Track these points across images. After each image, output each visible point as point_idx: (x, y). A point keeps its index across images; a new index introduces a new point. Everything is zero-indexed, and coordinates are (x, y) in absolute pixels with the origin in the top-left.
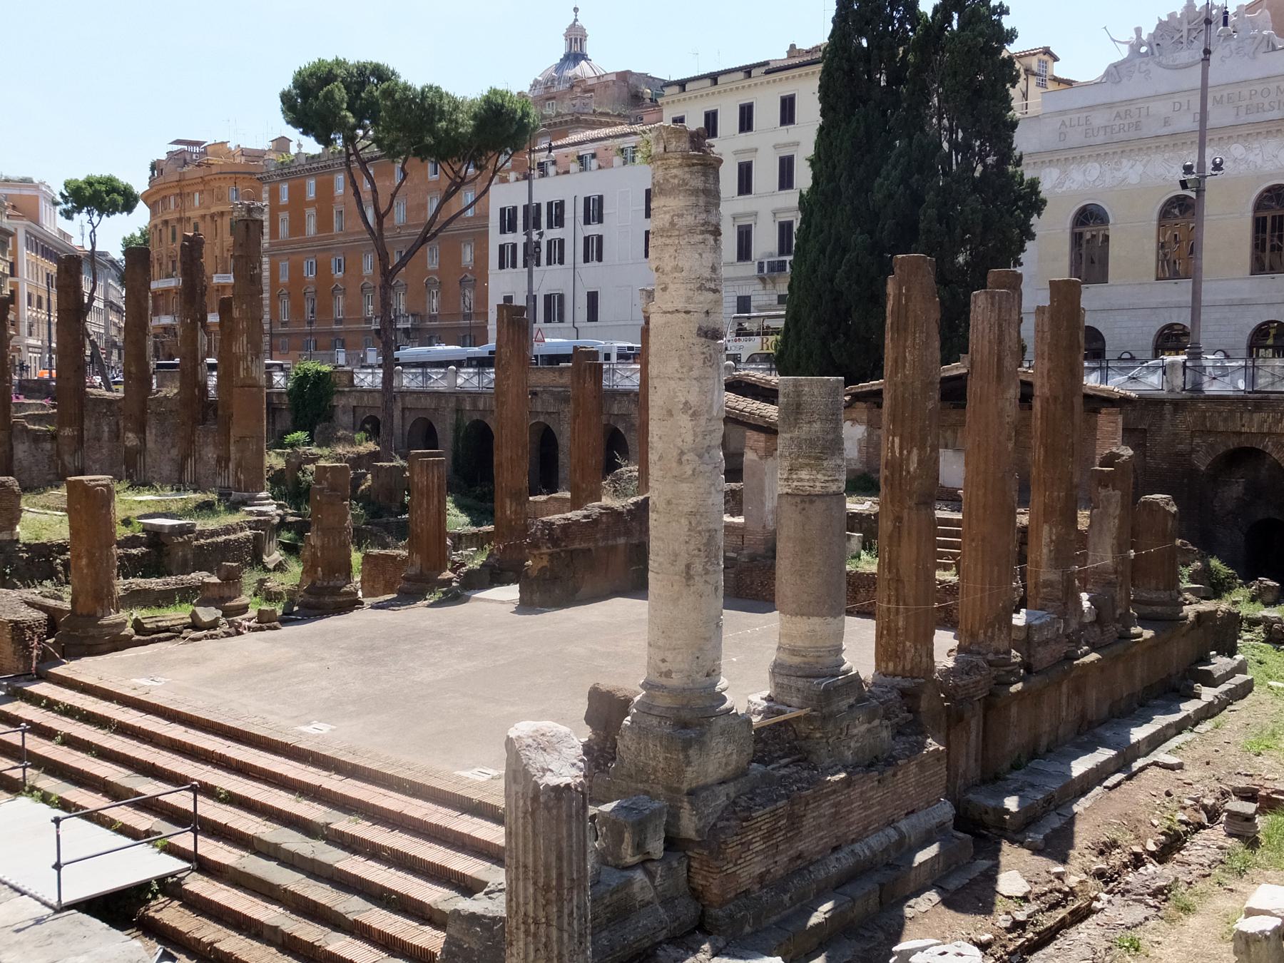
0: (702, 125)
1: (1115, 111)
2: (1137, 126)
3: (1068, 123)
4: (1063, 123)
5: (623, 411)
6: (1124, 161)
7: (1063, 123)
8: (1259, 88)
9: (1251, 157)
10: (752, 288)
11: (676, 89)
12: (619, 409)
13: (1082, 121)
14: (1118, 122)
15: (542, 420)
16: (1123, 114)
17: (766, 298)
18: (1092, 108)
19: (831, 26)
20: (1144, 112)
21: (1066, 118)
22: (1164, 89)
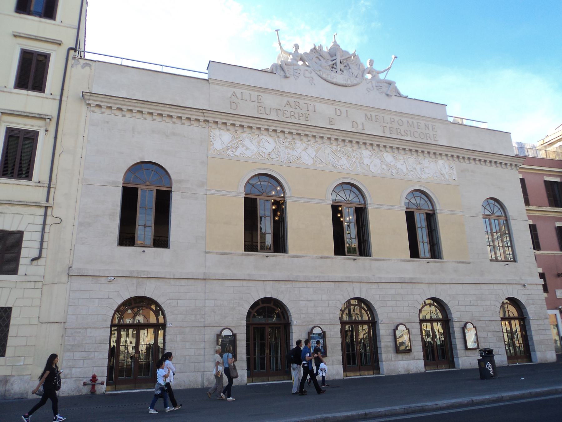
9: (399, 165)
21: (238, 91)
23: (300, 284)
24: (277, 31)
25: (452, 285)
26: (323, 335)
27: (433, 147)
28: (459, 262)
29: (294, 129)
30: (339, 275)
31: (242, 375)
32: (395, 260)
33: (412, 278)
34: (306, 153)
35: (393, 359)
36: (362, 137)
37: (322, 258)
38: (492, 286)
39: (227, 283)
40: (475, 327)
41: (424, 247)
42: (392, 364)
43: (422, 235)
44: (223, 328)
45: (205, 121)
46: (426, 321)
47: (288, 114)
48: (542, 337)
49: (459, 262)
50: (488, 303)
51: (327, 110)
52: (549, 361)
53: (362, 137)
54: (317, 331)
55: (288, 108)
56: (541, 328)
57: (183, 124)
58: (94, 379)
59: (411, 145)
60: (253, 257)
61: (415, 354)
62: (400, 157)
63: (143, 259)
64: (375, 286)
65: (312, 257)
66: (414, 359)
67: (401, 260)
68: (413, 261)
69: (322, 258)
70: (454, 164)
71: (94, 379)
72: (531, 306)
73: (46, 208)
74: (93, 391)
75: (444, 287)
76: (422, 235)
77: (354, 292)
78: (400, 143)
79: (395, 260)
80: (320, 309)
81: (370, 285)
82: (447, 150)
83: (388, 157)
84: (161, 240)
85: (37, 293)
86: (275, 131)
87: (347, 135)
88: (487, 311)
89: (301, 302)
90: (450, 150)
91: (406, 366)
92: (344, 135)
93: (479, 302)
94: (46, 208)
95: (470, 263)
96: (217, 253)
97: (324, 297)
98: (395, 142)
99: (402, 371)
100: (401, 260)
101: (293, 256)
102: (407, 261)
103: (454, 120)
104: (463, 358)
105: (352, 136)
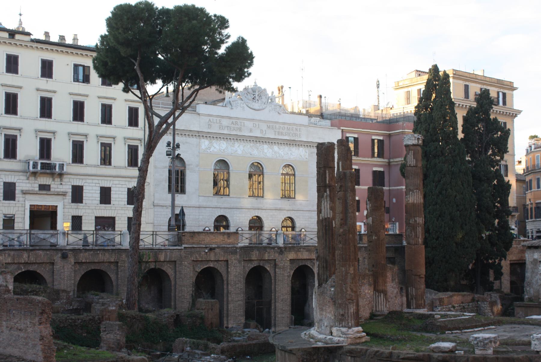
0: (515, 108)
1: (231, 120)
2: (240, 130)
3: (212, 120)
4: (210, 120)
5: (272, 257)
6: (236, 143)
7: (210, 120)
8: (282, 126)
9: (280, 152)
10: (17, 178)
11: (6, 35)
12: (269, 256)
13: (218, 121)
14: (233, 126)
15: (212, 266)
16: (234, 123)
17: (28, 185)
18: (223, 117)
19: (248, 45)
20: (242, 124)
21: (211, 118)
22: (250, 117)
39: (207, 209)
51: (249, 124)
64: (264, 211)
83: (276, 148)
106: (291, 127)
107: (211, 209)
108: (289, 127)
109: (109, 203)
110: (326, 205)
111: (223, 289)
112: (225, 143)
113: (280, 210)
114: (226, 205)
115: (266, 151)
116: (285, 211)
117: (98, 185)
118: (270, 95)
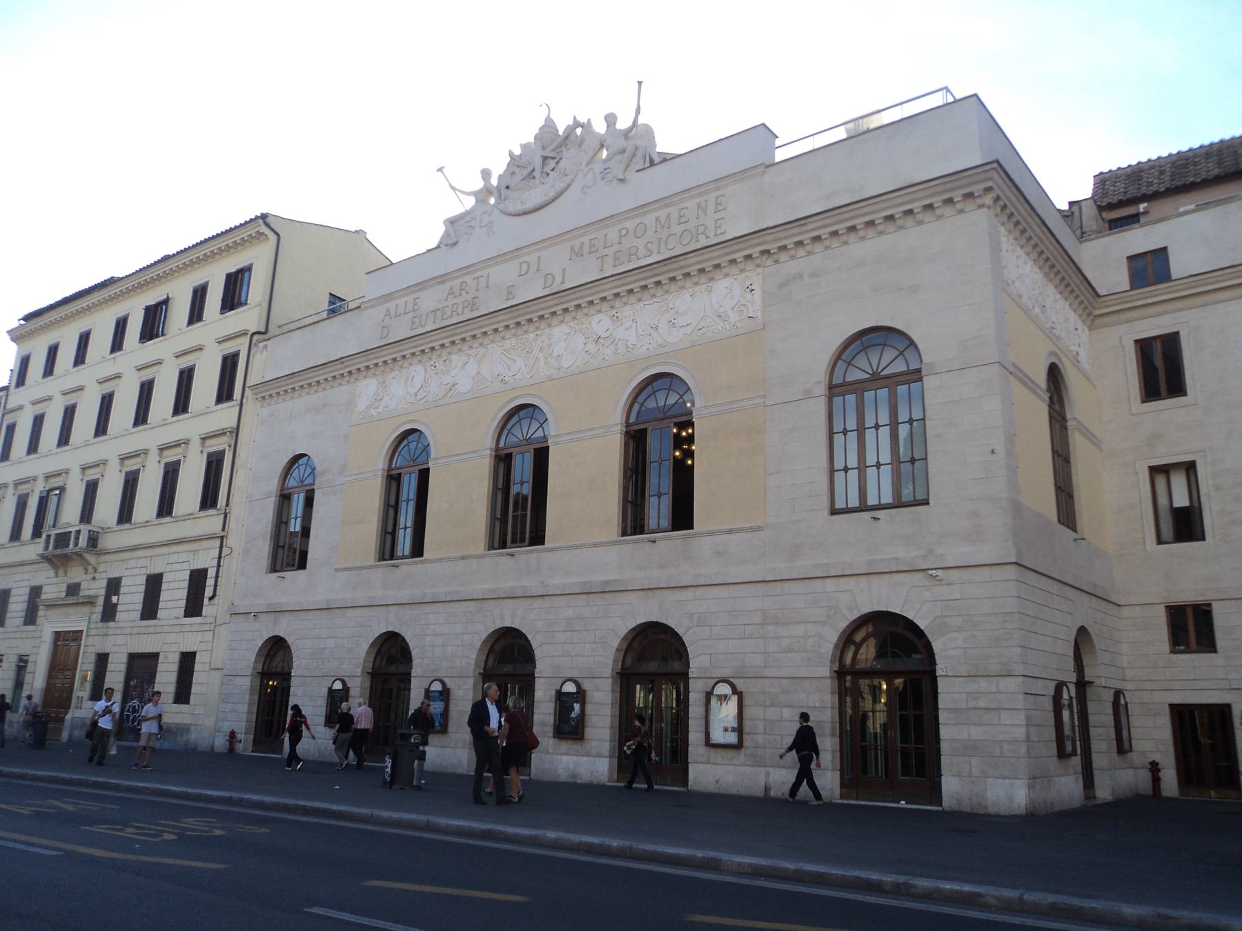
9: (620, 333)
16: (457, 290)
21: (391, 305)
23: (428, 608)
24: (440, 170)
25: (700, 591)
26: (445, 694)
27: (692, 259)
28: (730, 531)
29: (818, 228)
30: (480, 587)
31: (828, 778)
32: (584, 546)
33: (607, 582)
34: (725, 301)
35: (550, 750)
36: (544, 305)
37: (464, 558)
38: (818, 583)
39: (350, 613)
40: (740, 695)
41: (659, 508)
42: (554, 760)
43: (659, 480)
44: (714, 681)
45: (763, 252)
46: (848, 673)
47: (642, 251)
48: (976, 733)
49: (730, 531)
50: (798, 630)
51: (504, 274)
52: (991, 810)
53: (544, 305)
54: (437, 687)
55: (451, 301)
56: (981, 704)
57: (920, 223)
58: (232, 734)
59: (639, 276)
60: (639, 546)
61: (594, 744)
62: (626, 312)
63: (662, 551)
64: (538, 603)
65: (449, 559)
66: (588, 755)
67: (595, 545)
68: (628, 542)
69: (464, 558)
70: (755, 277)
71: (232, 734)
72: (954, 635)
73: (222, 538)
74: (232, 750)
75: (679, 595)
76: (659, 480)
77: (502, 617)
78: (616, 283)
79: (584, 546)
80: (449, 649)
81: (530, 601)
82: (726, 250)
83: (600, 323)
84: (682, 517)
85: (209, 636)
86: (890, 218)
87: (521, 312)
88: (790, 650)
89: (427, 638)
90: (736, 247)
91: (572, 766)
92: (515, 314)
93: (770, 628)
94: (222, 538)
95: (760, 529)
96: (345, 569)
97: (458, 628)
98: (608, 286)
99: (563, 776)
100: (595, 545)
101: (701, 534)
102: (370, 567)
103: (847, 131)
104: (701, 767)
105: (528, 310)
106: (674, 211)
107: (358, 612)
108: (663, 214)
109: (690, 526)
110: (73, 649)
111: (12, 849)
112: (420, 368)
113: (604, 591)
114: (405, 595)
115: (558, 349)
116: (632, 597)
117: (186, 566)
118: (470, 202)
